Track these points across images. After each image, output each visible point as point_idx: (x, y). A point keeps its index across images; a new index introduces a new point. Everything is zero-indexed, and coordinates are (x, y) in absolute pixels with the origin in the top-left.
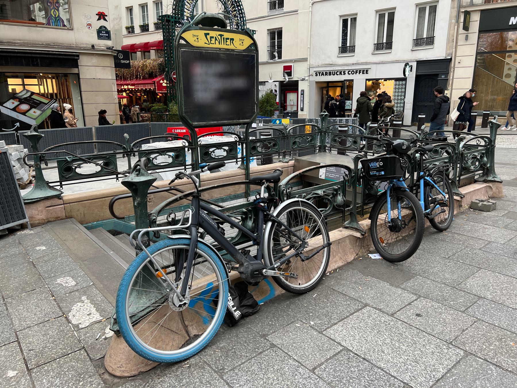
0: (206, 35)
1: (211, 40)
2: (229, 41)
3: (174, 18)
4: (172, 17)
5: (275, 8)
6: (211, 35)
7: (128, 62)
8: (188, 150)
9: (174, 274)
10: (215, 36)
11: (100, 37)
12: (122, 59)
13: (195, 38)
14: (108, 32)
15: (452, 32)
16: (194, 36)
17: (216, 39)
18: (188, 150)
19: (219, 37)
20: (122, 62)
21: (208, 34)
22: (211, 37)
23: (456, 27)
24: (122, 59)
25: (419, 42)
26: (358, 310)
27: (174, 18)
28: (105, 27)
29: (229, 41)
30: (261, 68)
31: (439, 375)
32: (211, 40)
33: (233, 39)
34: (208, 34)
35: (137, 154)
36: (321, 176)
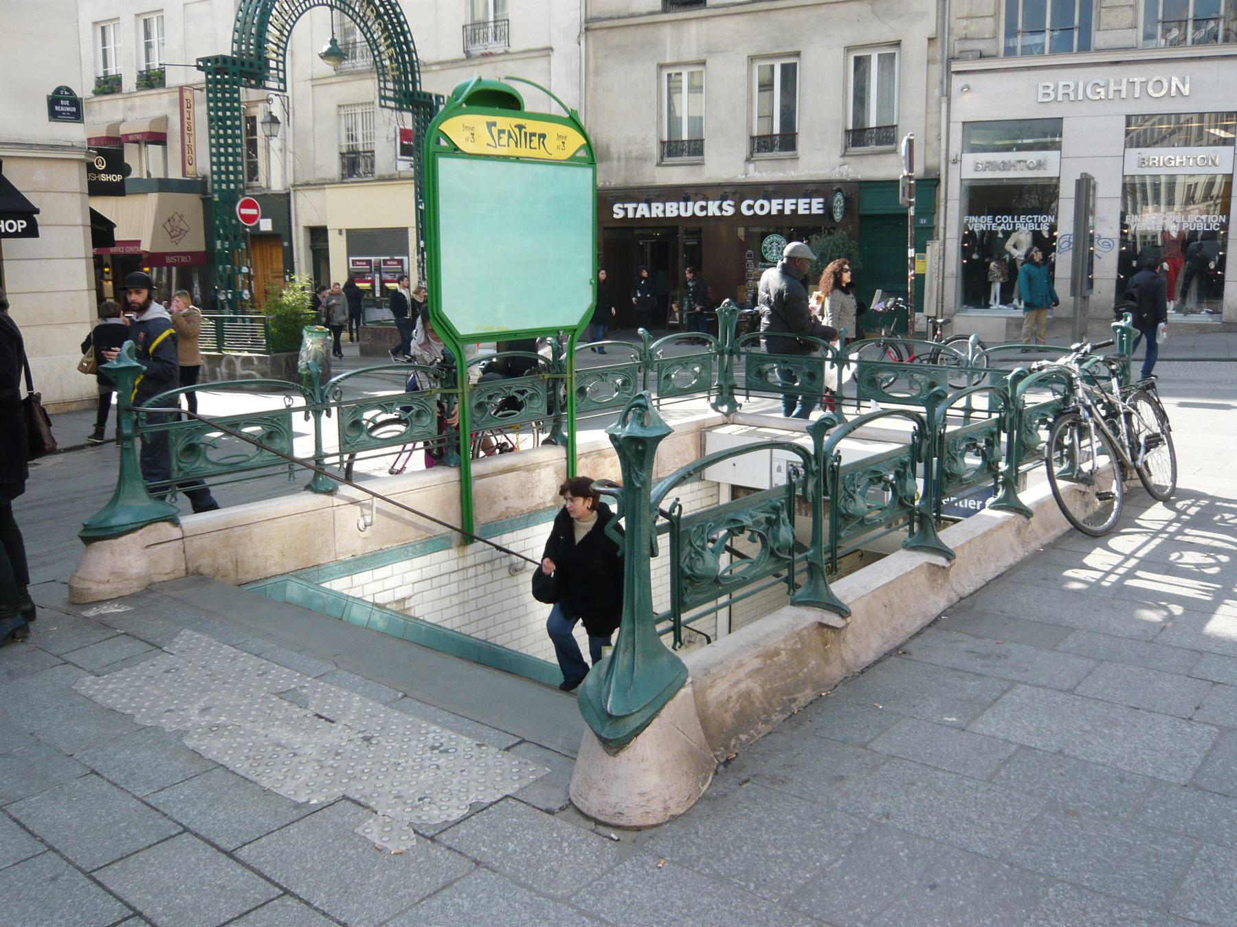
0: (490, 125)
1: (500, 138)
2: (535, 139)
3: (238, 64)
4: (234, 61)
5: (1060, 143)
6: (499, 127)
7: (119, 178)
8: (832, 367)
9: (672, 633)
10: (507, 128)
11: (54, 115)
12: (102, 172)
13: (468, 134)
14: (76, 102)
15: (932, 119)
16: (465, 127)
17: (510, 136)
18: (832, 367)
19: (517, 130)
20: (104, 178)
21: (494, 124)
22: (501, 132)
23: (944, 106)
24: (102, 172)
25: (858, 136)
26: (1005, 692)
27: (238, 64)
28: (68, 90)
29: (535, 139)
30: (170, 177)
31: (1197, 762)
32: (500, 138)
33: (543, 136)
34: (494, 124)
35: (334, 410)
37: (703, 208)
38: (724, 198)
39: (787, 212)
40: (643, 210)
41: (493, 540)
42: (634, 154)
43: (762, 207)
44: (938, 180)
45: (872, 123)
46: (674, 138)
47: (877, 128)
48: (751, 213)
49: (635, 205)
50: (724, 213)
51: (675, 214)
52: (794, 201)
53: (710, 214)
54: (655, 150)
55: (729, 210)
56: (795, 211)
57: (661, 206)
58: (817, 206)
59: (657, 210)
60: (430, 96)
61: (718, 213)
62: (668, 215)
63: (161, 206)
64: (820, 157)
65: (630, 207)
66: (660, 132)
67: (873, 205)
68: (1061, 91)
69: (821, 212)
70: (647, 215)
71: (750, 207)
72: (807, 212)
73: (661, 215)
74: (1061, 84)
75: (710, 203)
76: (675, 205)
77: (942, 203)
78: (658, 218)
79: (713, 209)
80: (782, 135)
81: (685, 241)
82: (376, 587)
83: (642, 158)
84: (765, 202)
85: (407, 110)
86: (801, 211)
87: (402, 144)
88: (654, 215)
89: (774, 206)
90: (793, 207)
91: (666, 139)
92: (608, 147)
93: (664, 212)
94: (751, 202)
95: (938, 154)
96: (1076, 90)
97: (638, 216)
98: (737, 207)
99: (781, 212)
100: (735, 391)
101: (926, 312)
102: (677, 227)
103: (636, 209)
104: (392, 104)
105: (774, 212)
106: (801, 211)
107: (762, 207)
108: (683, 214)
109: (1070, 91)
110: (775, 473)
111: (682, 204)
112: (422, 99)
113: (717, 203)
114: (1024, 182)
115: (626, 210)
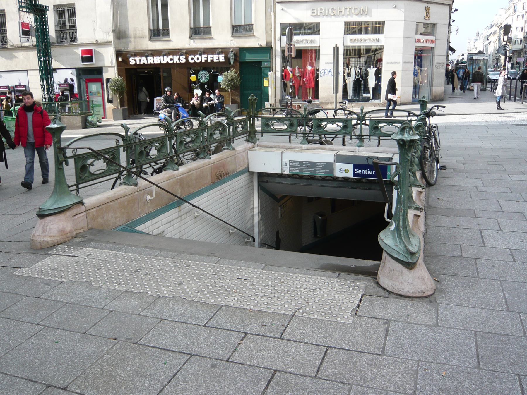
36: (284, 171)
37: (171, 59)
38: (181, 55)
39: (209, 61)
40: (144, 61)
41: (192, 202)
42: (138, 35)
43: (198, 59)
44: (272, 47)
45: (202, 25)
46: (197, 26)
47: (204, 28)
48: (193, 61)
49: (140, 58)
50: (181, 62)
51: (159, 62)
52: (212, 56)
53: (175, 62)
54: (147, 33)
55: (183, 61)
56: (212, 61)
57: (151, 58)
58: (222, 58)
59: (150, 60)
60: (43, 6)
61: (178, 62)
62: (156, 62)
63: (127, 44)
64: (222, 38)
65: (138, 59)
66: (190, 24)
67: (249, 58)
68: (319, 11)
69: (224, 61)
70: (146, 63)
71: (192, 59)
72: (218, 61)
73: (152, 63)
74: (319, 8)
75: (175, 57)
76: (158, 58)
77: (274, 57)
78: (151, 64)
79: (176, 60)
80: (163, 30)
81: (163, 75)
82: (151, 228)
83: (142, 37)
84: (199, 57)
85: (31, 13)
86: (215, 61)
87: (22, 29)
88: (149, 63)
89: (203, 58)
90: (212, 59)
91: (152, 28)
92: (125, 32)
93: (154, 61)
94: (193, 56)
95: (271, 36)
96: (325, 11)
97: (142, 63)
98: (187, 59)
99: (206, 61)
100: (256, 133)
101: (270, 102)
102: (160, 68)
103: (140, 60)
104: (24, 10)
105: (203, 61)
106: (215, 61)
107: (198, 59)
108: (163, 62)
109: (315, 11)
110: (284, 166)
111: (162, 58)
112: (39, 8)
113: (178, 57)
114: (308, 48)
115: (135, 60)
